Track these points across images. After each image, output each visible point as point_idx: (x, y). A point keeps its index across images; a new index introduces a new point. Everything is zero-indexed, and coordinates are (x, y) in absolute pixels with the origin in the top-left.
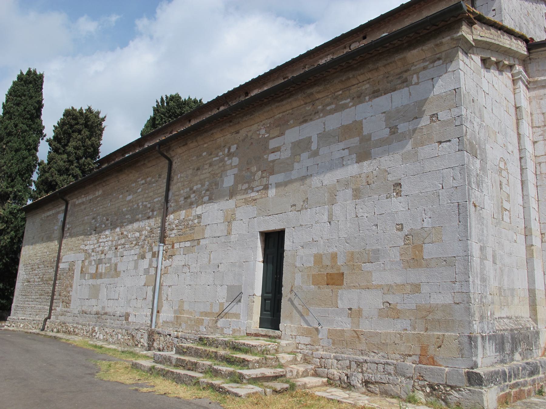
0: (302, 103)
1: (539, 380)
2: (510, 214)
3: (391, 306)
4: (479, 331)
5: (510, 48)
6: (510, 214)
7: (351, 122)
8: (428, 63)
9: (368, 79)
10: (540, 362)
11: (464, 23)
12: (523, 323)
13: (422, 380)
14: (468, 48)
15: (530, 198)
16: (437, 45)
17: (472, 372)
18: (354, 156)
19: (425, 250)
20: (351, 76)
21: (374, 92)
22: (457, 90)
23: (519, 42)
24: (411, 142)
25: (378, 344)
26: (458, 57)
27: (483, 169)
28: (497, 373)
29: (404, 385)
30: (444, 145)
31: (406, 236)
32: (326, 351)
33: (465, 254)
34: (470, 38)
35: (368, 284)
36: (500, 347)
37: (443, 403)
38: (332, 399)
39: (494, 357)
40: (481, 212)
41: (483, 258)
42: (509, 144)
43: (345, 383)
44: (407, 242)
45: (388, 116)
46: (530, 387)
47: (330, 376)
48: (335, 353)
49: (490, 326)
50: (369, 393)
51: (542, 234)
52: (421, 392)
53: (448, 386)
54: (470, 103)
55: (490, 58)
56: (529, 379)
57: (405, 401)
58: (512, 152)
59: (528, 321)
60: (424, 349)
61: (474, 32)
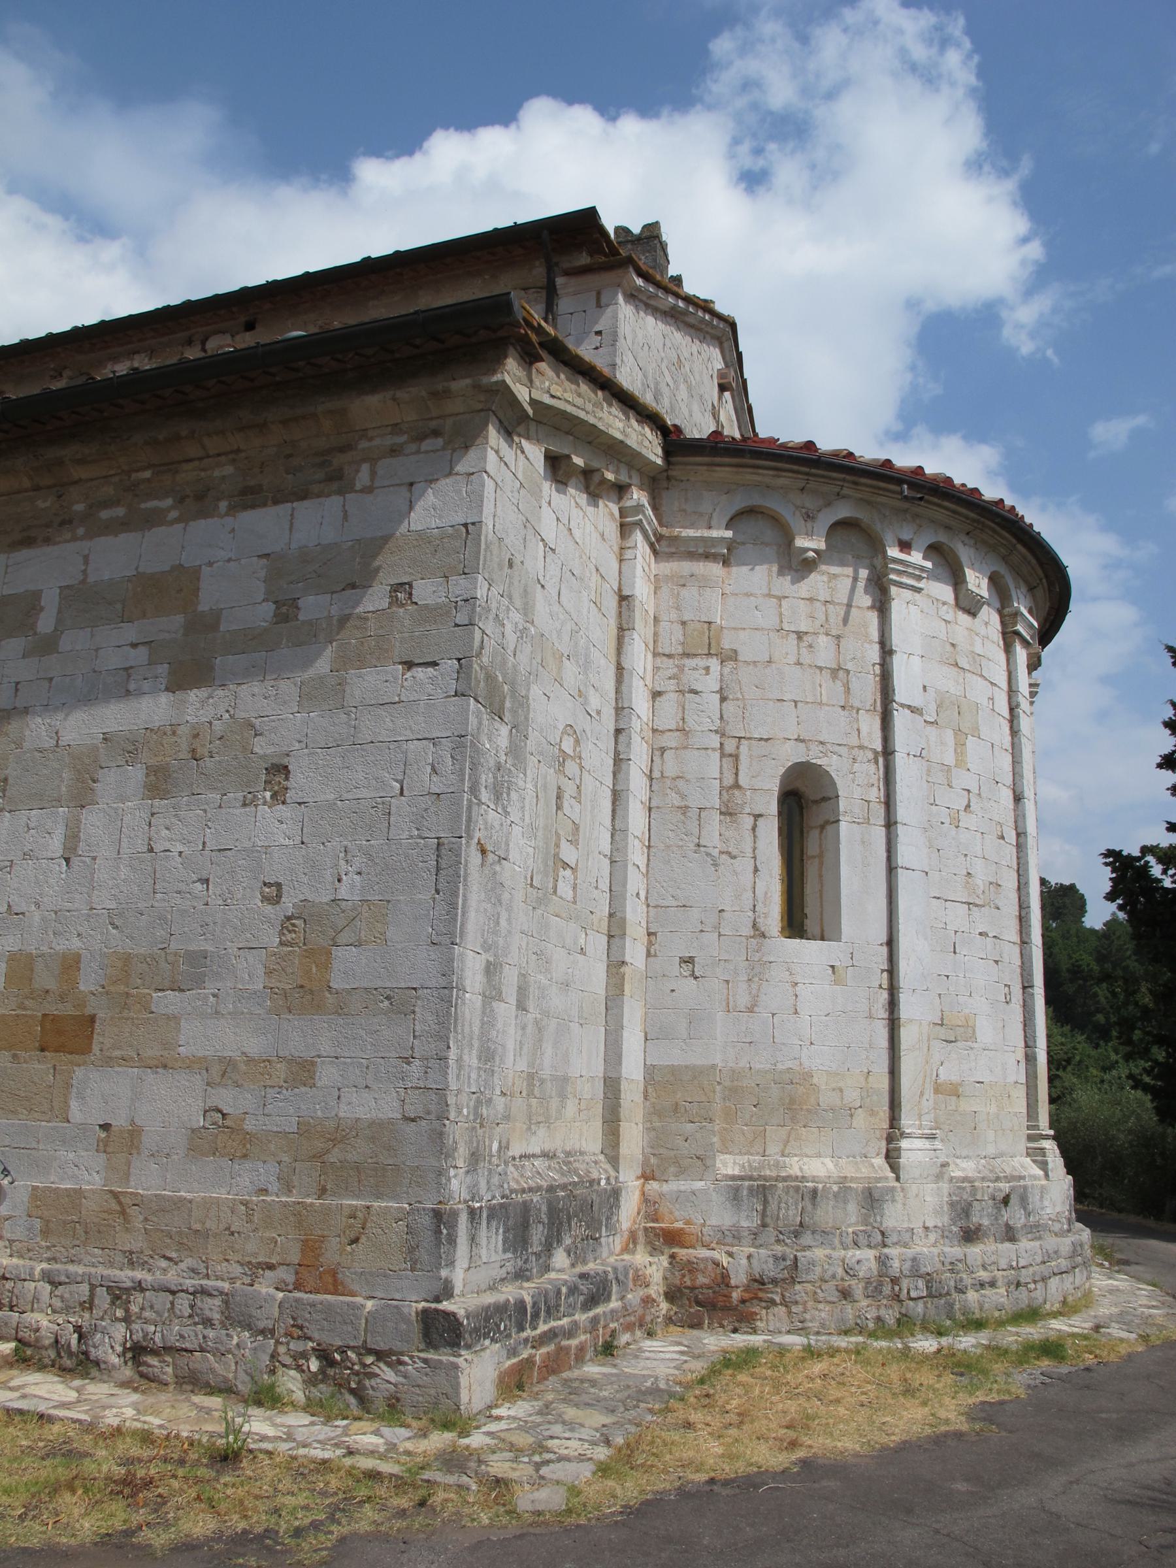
0: (27, 483)
1: (609, 1317)
2: (576, 878)
3: (227, 1123)
4: (465, 1195)
5: (622, 442)
6: (576, 878)
7: (168, 569)
8: (404, 438)
9: (231, 452)
10: (615, 1269)
11: (511, 350)
12: (581, 1168)
13: (299, 1338)
14: (517, 421)
15: (631, 838)
16: (434, 395)
17: (436, 1310)
18: (163, 669)
19: (335, 964)
20: (184, 433)
21: (245, 491)
22: (470, 527)
23: (647, 430)
24: (329, 652)
25: (180, 1233)
26: (486, 438)
27: (516, 751)
28: (501, 1309)
29: (247, 1353)
30: (419, 672)
31: (289, 918)
32: (21, 1257)
33: (443, 982)
34: (523, 394)
35: (165, 1053)
36: (517, 1240)
37: (352, 1400)
38: (21, 1412)
39: (498, 1265)
40: (498, 868)
41: (493, 994)
42: (592, 691)
43: (71, 1354)
44: (289, 937)
45: (278, 567)
46: (583, 1338)
47: (25, 1334)
48: (49, 1260)
49: (495, 1180)
50: (143, 1381)
51: (649, 934)
52: (292, 1373)
53: (370, 1351)
54: (501, 568)
55: (568, 457)
56: (582, 1317)
57: (245, 1402)
58: (599, 713)
59: (596, 1162)
60: (311, 1248)
61: (537, 382)
